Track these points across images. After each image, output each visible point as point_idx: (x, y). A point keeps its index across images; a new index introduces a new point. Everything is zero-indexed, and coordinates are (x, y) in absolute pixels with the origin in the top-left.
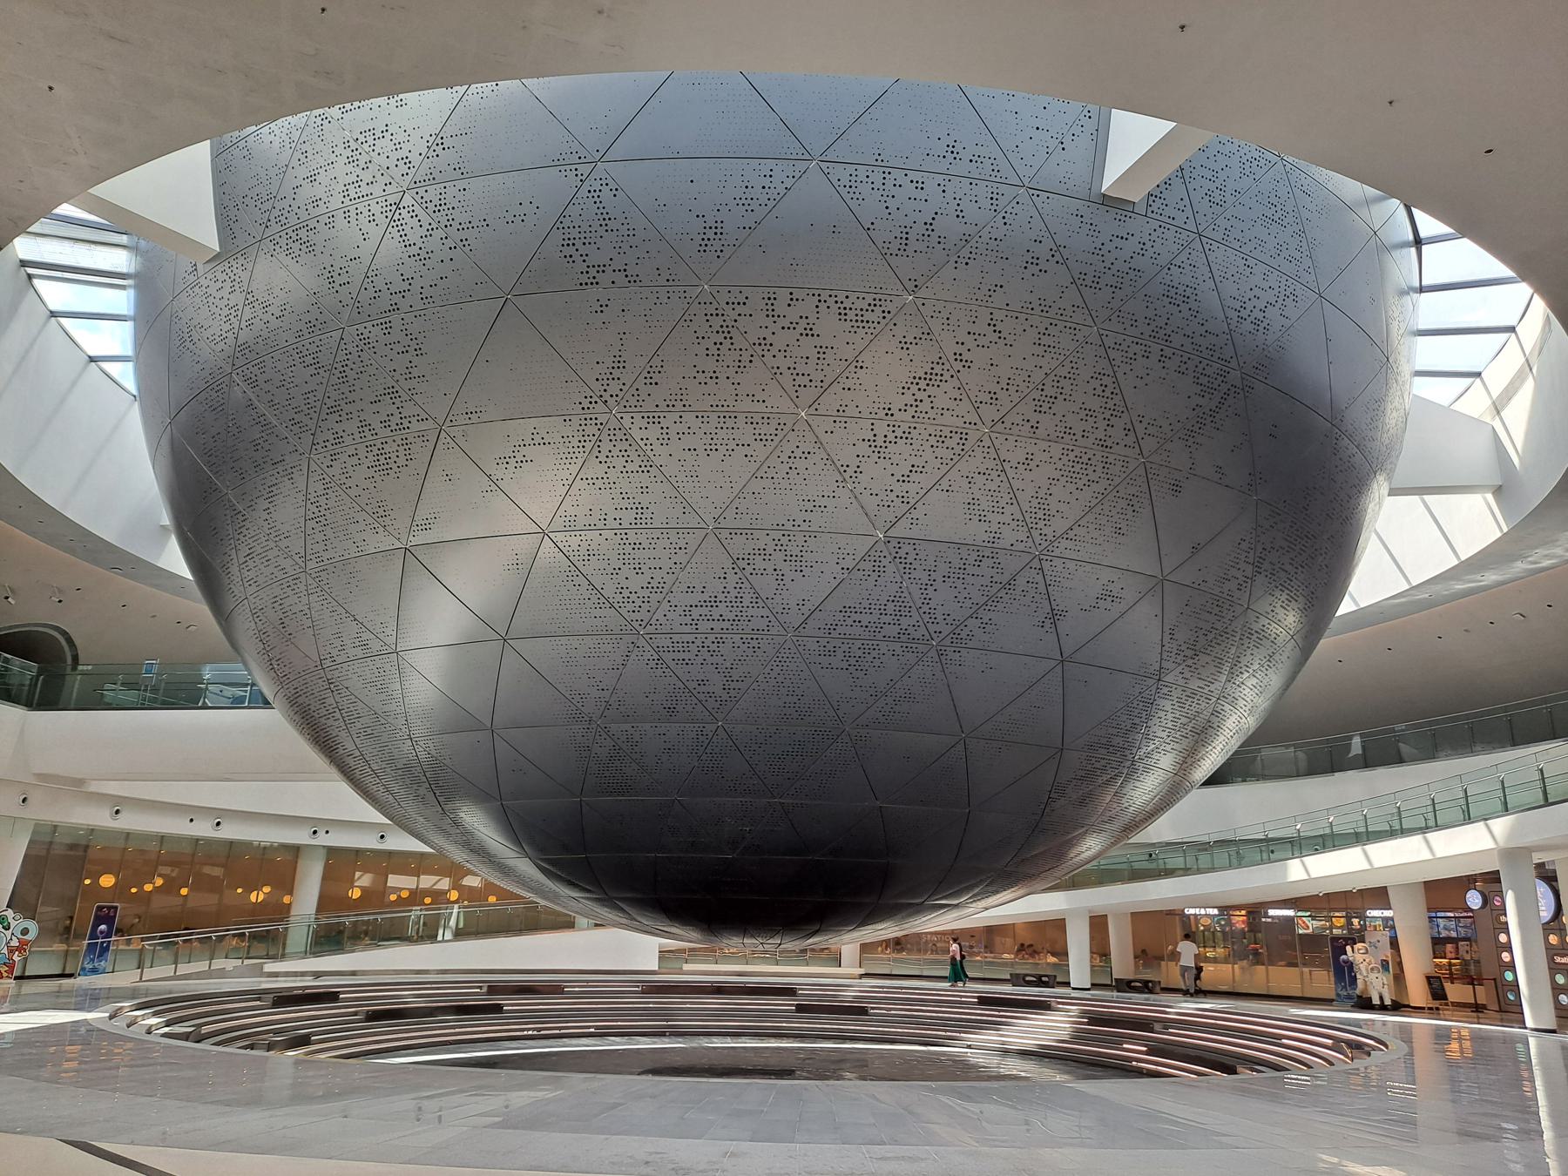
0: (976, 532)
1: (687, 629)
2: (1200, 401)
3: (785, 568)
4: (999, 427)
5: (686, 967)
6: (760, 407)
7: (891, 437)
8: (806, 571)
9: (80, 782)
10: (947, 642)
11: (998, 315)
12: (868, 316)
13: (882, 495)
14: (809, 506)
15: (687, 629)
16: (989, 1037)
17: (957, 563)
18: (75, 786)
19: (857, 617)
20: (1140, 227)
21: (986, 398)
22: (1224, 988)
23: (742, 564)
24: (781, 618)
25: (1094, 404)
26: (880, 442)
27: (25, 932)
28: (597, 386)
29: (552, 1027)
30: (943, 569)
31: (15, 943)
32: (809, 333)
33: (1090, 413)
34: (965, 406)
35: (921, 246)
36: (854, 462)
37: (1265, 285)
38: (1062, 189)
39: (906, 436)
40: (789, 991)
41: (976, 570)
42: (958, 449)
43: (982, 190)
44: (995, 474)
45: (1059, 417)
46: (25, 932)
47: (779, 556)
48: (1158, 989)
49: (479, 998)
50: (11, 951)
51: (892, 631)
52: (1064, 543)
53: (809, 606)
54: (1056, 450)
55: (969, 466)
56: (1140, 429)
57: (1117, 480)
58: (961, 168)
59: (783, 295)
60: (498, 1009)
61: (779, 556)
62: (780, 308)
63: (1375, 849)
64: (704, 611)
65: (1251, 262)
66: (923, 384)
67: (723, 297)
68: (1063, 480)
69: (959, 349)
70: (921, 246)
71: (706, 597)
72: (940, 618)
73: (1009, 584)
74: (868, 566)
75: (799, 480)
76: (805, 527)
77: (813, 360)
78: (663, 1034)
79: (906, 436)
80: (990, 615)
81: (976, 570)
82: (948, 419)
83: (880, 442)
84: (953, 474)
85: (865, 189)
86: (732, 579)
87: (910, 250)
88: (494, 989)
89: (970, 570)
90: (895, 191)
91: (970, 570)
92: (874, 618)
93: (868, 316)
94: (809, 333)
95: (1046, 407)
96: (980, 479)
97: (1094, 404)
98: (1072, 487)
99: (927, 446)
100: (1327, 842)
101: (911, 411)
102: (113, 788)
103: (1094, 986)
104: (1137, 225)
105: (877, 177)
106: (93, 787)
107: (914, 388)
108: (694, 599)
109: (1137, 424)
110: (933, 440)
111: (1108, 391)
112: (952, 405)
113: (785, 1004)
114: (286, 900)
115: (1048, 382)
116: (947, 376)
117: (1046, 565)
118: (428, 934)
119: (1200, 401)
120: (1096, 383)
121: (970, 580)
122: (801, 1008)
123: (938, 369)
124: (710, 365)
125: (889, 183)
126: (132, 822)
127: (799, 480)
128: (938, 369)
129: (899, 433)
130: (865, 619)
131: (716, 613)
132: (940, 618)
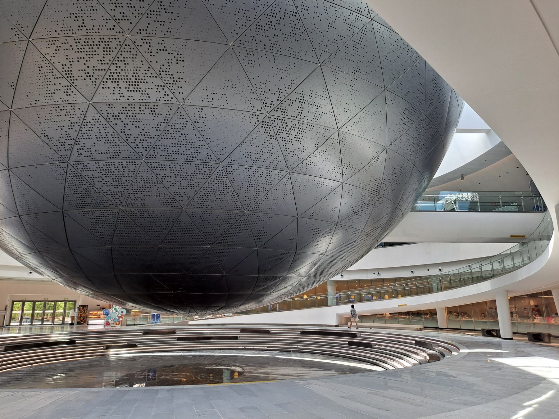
27: (122, 312)
29: (250, 346)
31: (120, 315)
46: (122, 312)
50: (119, 317)
113: (345, 340)
118: (455, 311)
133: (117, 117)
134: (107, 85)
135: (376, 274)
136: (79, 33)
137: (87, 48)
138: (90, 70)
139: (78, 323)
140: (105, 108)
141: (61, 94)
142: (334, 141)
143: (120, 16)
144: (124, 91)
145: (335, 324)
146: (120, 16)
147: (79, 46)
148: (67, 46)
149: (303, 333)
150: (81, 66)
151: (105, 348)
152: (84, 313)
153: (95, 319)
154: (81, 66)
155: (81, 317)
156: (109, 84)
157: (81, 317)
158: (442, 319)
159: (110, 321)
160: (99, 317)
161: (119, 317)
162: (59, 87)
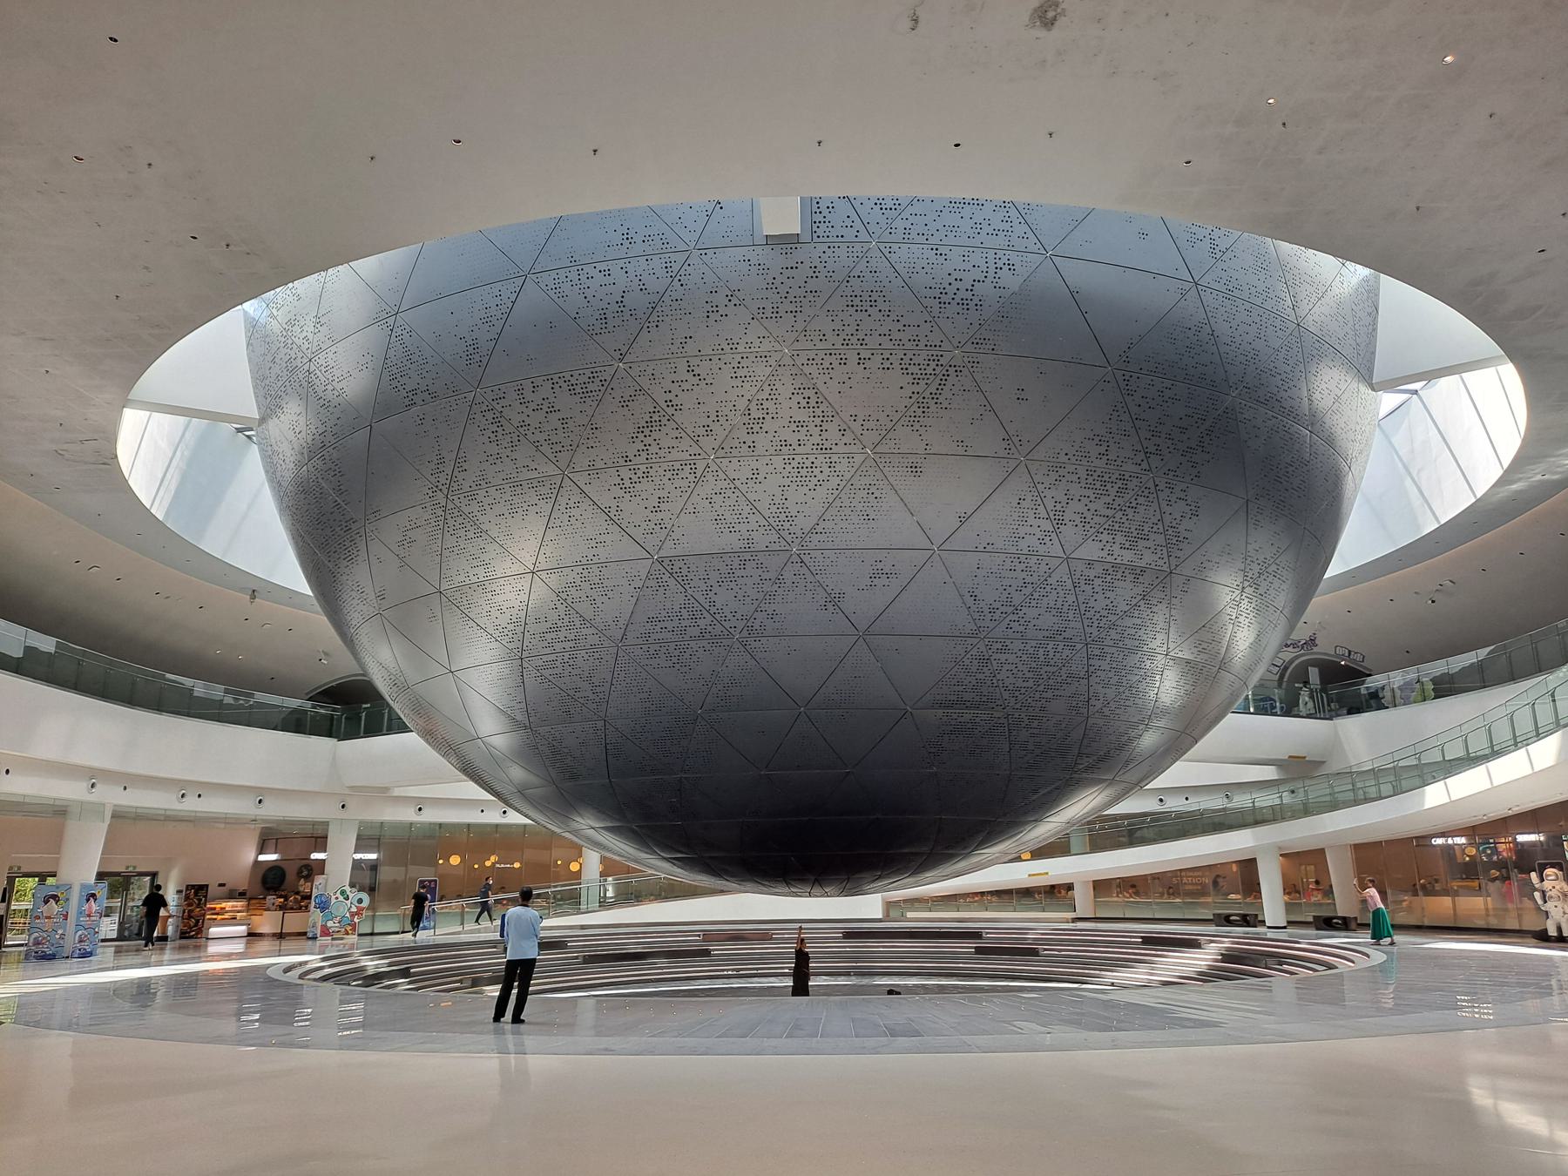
0: (731, 541)
1: (548, 651)
2: (916, 388)
3: (594, 594)
4: (721, 453)
5: (910, 915)
6: (535, 474)
7: (635, 478)
8: (610, 594)
9: (387, 789)
10: (745, 633)
11: (694, 362)
12: (591, 387)
13: (644, 525)
14: (593, 543)
15: (548, 651)
16: (1138, 975)
17: (724, 570)
18: (382, 793)
19: (663, 624)
20: (809, 254)
21: (702, 431)
22: (1480, 923)
23: (564, 596)
24: (608, 633)
25: (801, 415)
26: (627, 484)
27: (360, 901)
28: (432, 479)
29: (750, 968)
30: (714, 576)
31: (354, 909)
32: (552, 410)
33: (800, 424)
34: (687, 442)
35: (618, 322)
36: (614, 504)
37: (969, 266)
38: (726, 242)
39: (647, 475)
40: (975, 935)
41: (742, 572)
42: (692, 478)
43: (657, 263)
44: (729, 493)
45: (771, 433)
46: (360, 901)
47: (585, 586)
48: (1353, 925)
49: (694, 942)
50: (353, 915)
51: (695, 632)
52: (815, 538)
53: (622, 621)
54: (778, 462)
55: (707, 488)
56: (856, 427)
57: (848, 476)
58: (638, 248)
59: (528, 385)
60: (707, 953)
61: (585, 586)
62: (529, 396)
63: (1496, 765)
64: (553, 635)
65: (942, 250)
66: (647, 432)
67: (490, 396)
68: (794, 486)
69: (669, 396)
70: (618, 322)
71: (549, 625)
72: (730, 616)
73: (778, 580)
74: (653, 583)
75: (579, 524)
76: (595, 560)
77: (560, 431)
78: (848, 974)
79: (647, 475)
80: (773, 607)
81: (742, 572)
82: (675, 455)
83: (627, 484)
84: (695, 498)
85: (566, 287)
86: (562, 608)
87: (610, 328)
88: (709, 936)
89: (738, 573)
90: (589, 283)
91: (738, 573)
92: (676, 623)
93: (591, 387)
94: (552, 410)
95: (756, 428)
96: (718, 499)
97: (801, 415)
98: (805, 490)
99: (665, 480)
100: (1450, 767)
101: (644, 455)
102: (413, 792)
103: (1290, 923)
104: (801, 254)
105: (573, 275)
106: (397, 792)
107: (641, 436)
108: (544, 627)
109: (852, 424)
110: (669, 475)
111: (813, 403)
112: (674, 443)
113: (968, 946)
114: (574, 867)
115: (753, 407)
116: (664, 421)
117: (806, 559)
118: (1101, 887)
119: (916, 388)
120: (796, 398)
121: (740, 581)
122: (979, 950)
123: (656, 417)
124: (493, 449)
125: (583, 278)
126: (431, 816)
127: (579, 524)
128: (656, 417)
129: (640, 474)
130: (669, 625)
131: (561, 635)
132: (730, 616)
133: (1088, 581)
134: (1101, 537)
135: (85, 785)
136: (1097, 463)
137: (1098, 485)
138: (1089, 516)
139: (183, 935)
140: (1080, 566)
141: (1033, 541)
142: (1204, 630)
143: (1152, 449)
144: (1116, 547)
145: (880, 916)
146: (1152, 449)
147: (1090, 480)
148: (1075, 478)
149: (849, 935)
150: (1080, 507)
151: (469, 983)
152: (198, 905)
153: (225, 923)
154: (1080, 507)
155: (190, 917)
156: (1105, 537)
157: (190, 917)
158: (1083, 900)
159: (330, 924)
160: (233, 921)
161: (353, 915)
162: (1036, 530)
